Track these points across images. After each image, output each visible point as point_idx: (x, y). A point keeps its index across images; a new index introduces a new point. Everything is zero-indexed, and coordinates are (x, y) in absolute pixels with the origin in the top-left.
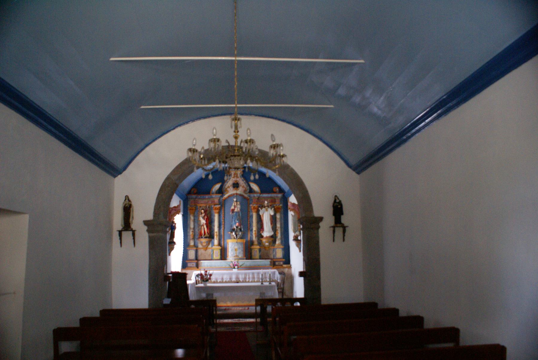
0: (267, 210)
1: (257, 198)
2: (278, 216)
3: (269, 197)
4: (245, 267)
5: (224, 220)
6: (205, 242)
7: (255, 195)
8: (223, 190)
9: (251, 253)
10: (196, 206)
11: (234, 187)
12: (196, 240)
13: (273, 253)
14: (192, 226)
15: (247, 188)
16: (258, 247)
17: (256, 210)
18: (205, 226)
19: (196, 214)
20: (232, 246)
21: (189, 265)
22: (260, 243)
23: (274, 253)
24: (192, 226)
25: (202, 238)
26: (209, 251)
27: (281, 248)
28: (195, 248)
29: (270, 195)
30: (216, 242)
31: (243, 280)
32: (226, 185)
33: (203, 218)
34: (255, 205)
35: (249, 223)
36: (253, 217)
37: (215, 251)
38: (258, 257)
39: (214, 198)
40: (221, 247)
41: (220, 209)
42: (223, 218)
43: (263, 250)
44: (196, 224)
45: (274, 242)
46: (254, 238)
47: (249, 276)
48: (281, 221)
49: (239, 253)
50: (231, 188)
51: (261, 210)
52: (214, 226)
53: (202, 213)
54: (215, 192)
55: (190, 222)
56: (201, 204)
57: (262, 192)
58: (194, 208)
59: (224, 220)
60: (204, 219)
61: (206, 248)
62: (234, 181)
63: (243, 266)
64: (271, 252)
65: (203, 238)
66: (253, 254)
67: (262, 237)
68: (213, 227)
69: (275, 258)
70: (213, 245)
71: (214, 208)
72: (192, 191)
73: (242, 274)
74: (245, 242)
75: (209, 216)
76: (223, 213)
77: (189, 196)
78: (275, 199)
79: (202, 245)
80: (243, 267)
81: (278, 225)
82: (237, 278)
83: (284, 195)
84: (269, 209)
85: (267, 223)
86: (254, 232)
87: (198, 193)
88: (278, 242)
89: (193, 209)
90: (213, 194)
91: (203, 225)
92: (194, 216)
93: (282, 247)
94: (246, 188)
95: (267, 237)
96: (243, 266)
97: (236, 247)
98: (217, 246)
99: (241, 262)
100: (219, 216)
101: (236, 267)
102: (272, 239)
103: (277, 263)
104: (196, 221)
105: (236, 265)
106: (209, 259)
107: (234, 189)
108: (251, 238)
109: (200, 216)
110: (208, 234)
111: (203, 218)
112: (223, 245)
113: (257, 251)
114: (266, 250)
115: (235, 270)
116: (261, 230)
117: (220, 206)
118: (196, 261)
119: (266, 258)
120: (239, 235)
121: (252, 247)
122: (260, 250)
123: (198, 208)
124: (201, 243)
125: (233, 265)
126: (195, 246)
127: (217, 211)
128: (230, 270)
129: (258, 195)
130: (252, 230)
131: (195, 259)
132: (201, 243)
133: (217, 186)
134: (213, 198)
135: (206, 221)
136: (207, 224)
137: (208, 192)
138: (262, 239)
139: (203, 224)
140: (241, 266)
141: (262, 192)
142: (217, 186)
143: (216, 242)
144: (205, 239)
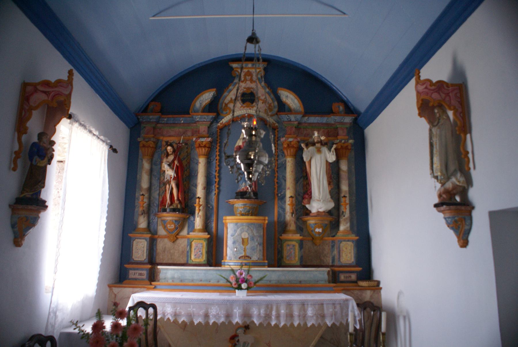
0: (319, 151)
1: (296, 123)
2: (344, 166)
3: (323, 124)
4: (268, 286)
5: (219, 173)
6: (172, 222)
7: (292, 117)
8: (220, 106)
9: (280, 252)
10: (158, 140)
11: (243, 101)
12: (152, 217)
13: (332, 251)
14: (145, 184)
15: (272, 105)
16: (298, 237)
17: (292, 150)
18: (173, 184)
19: (156, 156)
20: (235, 231)
21: (132, 274)
22: (301, 227)
23: (335, 252)
24: (145, 184)
25: (165, 210)
26: (182, 243)
27: (353, 241)
28: (148, 236)
29: (324, 120)
30: (198, 221)
31: (261, 320)
32: (226, 97)
33: (171, 165)
34: (290, 140)
35: (276, 180)
36: (285, 168)
37: (194, 244)
38: (296, 260)
39: (198, 121)
40: (209, 234)
41: (210, 149)
42: (218, 169)
43: (308, 245)
44: (155, 182)
45: (335, 225)
46: (289, 217)
47: (278, 311)
48: (349, 179)
49: (253, 249)
50: (239, 104)
51: (305, 149)
52: (196, 186)
53: (168, 155)
54: (201, 109)
55: (141, 176)
56: (170, 136)
57: (308, 111)
58: (152, 144)
59: (219, 173)
60: (173, 169)
61: (175, 237)
62: (245, 88)
63: (260, 283)
64: (327, 248)
65: (168, 210)
66: (285, 253)
67: (308, 213)
68: (194, 188)
69: (336, 263)
70: (192, 229)
71: (197, 145)
72: (151, 107)
73: (258, 304)
74: (268, 224)
75: (184, 163)
76: (218, 158)
77: (144, 118)
78: (336, 129)
79: (165, 227)
80: (260, 286)
81: (345, 187)
82: (246, 315)
83: (355, 121)
84: (325, 149)
85: (319, 181)
86: (288, 201)
87: (163, 112)
88: (343, 227)
89: (149, 146)
90: (196, 111)
91: (169, 182)
92: (152, 163)
93: (354, 237)
94: (270, 105)
95: (319, 214)
96: (260, 283)
97: (245, 235)
98: (200, 231)
99: (257, 273)
100: (209, 164)
101: (244, 286)
102: (330, 218)
103: (342, 277)
104: (155, 173)
105: (244, 281)
106: (182, 262)
107: (244, 105)
108: (279, 215)
109: (165, 160)
110: (180, 202)
111: (169, 165)
112: (214, 230)
113: (294, 246)
114: (315, 244)
115: (241, 295)
116: (303, 198)
117: (209, 139)
118: (150, 266)
119: (315, 263)
120: (260, 163)
121: (284, 236)
122: (301, 244)
123: (161, 147)
124: (164, 224)
125: (237, 281)
126: (151, 230)
127: (204, 151)
128: (229, 291)
129: (299, 117)
130: (283, 198)
131: (147, 261)
132: (164, 224)
133: (207, 97)
134: (196, 122)
135: (177, 172)
136: (177, 179)
137: (185, 110)
138: (306, 218)
139: (168, 178)
140: (255, 283)
141: (308, 111)
142: (207, 97)
143: (198, 221)
144: (172, 214)
